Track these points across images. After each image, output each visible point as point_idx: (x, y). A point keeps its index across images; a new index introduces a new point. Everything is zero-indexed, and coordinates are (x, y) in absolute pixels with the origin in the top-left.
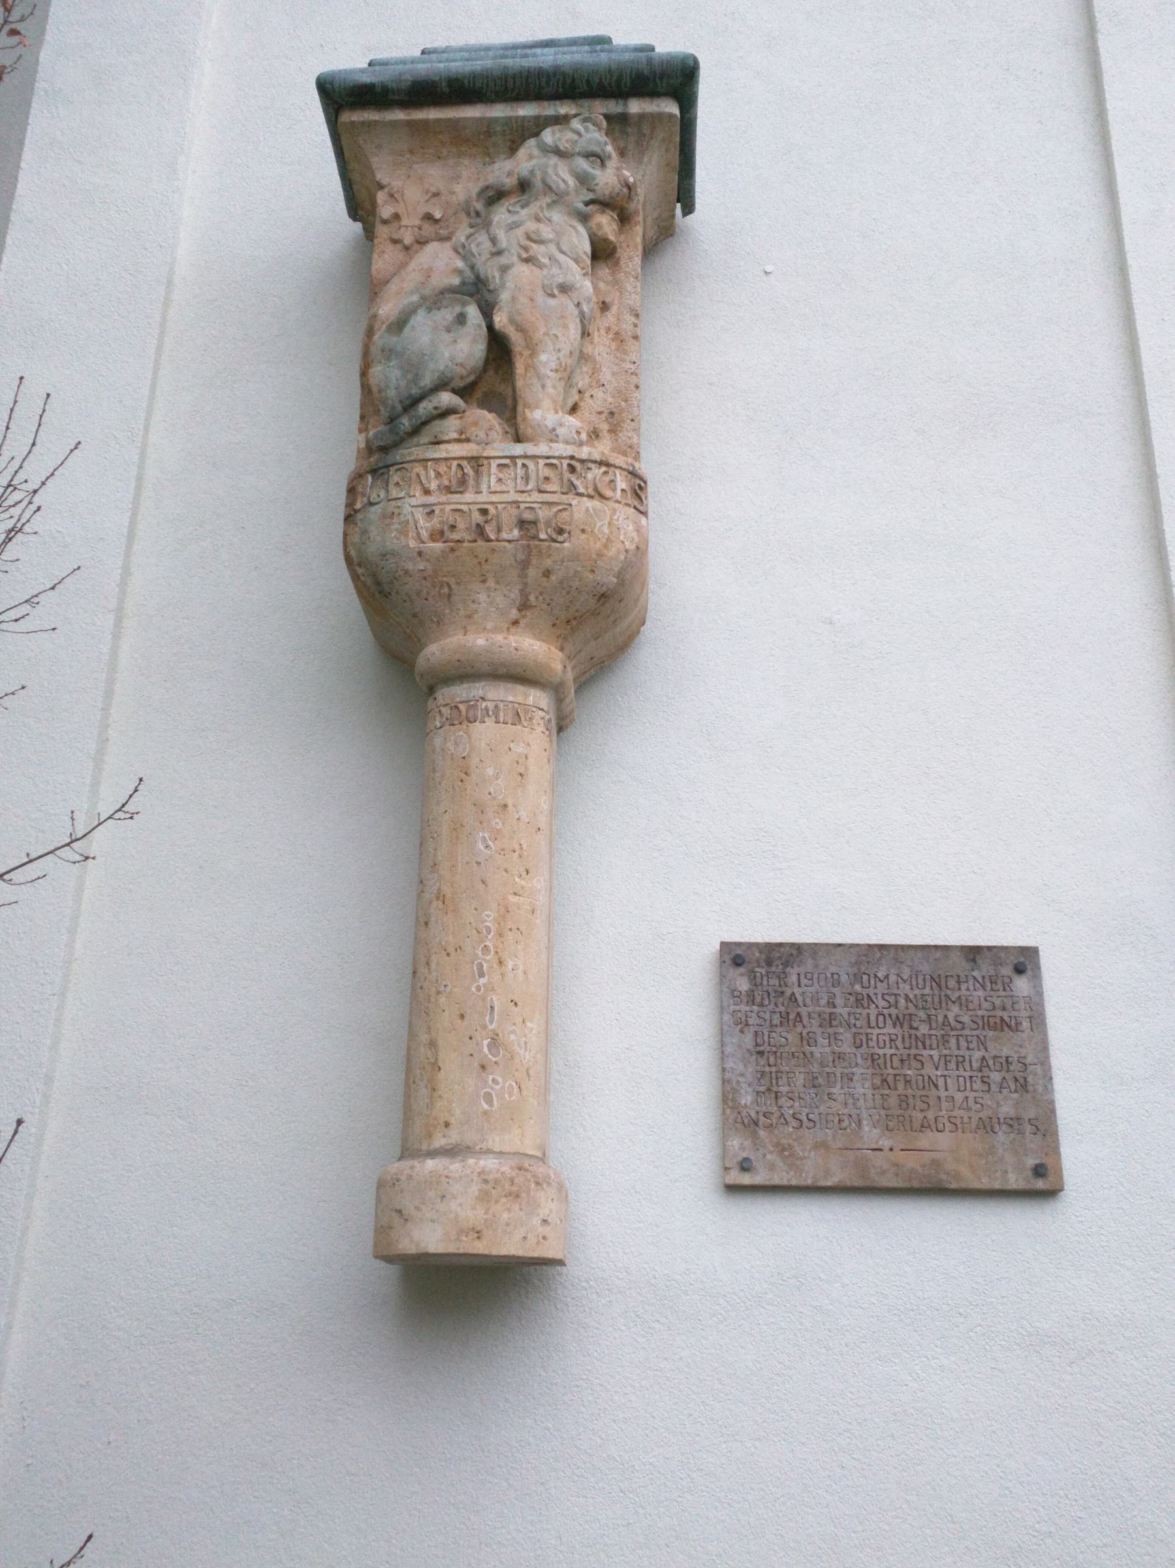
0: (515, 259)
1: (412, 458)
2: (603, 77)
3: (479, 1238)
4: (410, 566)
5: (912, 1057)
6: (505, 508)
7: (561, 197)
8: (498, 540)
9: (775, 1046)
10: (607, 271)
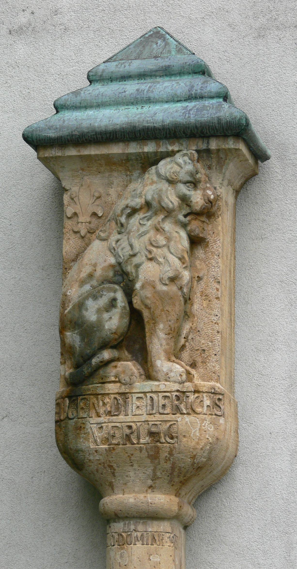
0: (144, 258)
1: (90, 393)
2: (193, 130)
4: (91, 458)
6: (141, 424)
7: (170, 213)
8: (138, 444)
10: (201, 251)
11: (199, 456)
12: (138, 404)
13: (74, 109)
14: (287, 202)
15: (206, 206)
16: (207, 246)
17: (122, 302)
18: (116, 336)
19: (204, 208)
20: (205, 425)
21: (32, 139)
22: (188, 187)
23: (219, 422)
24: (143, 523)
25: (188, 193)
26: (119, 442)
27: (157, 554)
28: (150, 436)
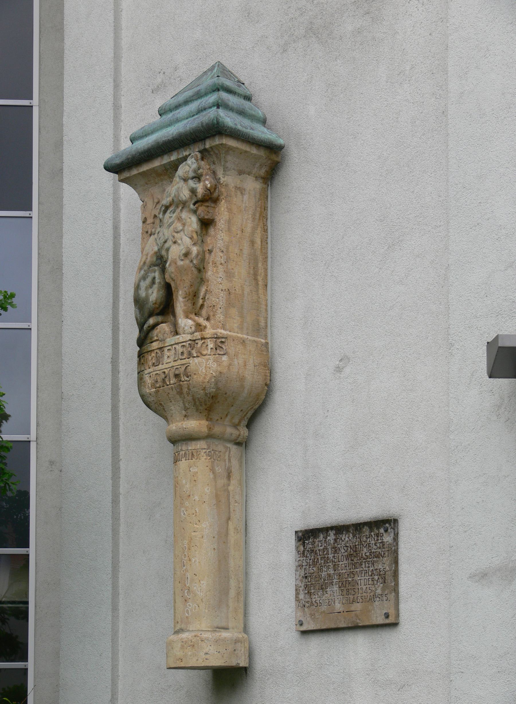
3: (182, 661)
5: (351, 573)
6: (170, 370)
9: (310, 574)
11: (208, 388)
12: (168, 354)
13: (140, 139)
14: (301, 179)
15: (205, 194)
16: (215, 225)
17: (158, 279)
18: (157, 306)
19: (204, 195)
20: (209, 363)
21: (109, 168)
22: (194, 181)
23: (221, 360)
24: (186, 443)
25: (194, 186)
26: (160, 385)
27: (195, 466)
28: (175, 377)
